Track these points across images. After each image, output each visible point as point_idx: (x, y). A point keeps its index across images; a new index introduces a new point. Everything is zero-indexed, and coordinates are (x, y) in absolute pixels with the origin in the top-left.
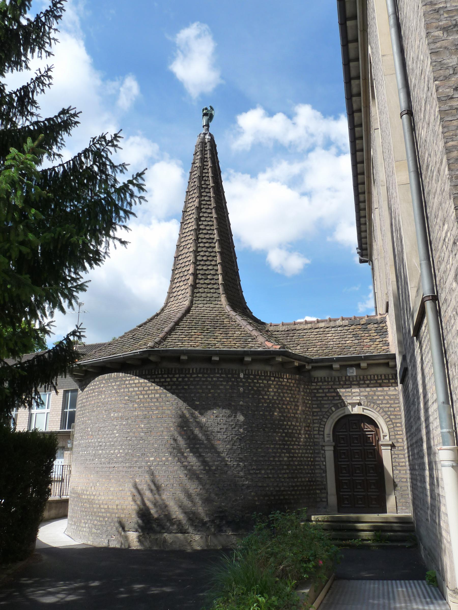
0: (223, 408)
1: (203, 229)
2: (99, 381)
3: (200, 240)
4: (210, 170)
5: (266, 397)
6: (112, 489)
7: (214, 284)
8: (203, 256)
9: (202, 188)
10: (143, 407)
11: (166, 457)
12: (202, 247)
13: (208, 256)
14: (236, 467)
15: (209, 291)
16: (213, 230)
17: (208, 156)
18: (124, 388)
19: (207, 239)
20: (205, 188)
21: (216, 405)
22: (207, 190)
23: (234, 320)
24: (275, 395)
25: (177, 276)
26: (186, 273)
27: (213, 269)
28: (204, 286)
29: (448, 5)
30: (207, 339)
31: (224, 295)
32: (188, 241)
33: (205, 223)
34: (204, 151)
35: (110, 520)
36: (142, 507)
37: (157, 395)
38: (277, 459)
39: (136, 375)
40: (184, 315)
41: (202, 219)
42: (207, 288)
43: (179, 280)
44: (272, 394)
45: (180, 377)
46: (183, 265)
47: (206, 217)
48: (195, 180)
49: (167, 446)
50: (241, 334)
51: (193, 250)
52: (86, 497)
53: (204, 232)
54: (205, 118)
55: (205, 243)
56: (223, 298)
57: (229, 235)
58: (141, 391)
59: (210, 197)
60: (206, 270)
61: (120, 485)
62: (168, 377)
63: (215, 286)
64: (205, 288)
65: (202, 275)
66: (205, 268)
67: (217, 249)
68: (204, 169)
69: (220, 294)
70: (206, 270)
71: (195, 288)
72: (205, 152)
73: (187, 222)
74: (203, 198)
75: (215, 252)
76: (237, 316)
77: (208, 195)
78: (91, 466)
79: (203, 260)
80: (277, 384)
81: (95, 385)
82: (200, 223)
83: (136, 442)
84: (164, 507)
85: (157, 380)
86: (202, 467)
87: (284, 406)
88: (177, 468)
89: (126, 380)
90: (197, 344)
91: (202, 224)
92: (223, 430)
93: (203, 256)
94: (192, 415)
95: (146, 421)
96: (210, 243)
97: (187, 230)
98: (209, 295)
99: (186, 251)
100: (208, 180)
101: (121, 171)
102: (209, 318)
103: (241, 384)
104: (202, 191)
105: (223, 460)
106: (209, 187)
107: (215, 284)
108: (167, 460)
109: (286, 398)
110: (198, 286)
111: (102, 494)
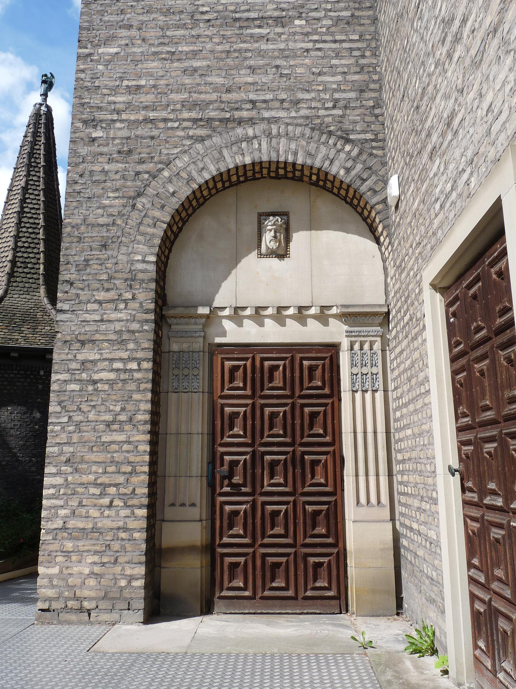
0: (19, 405)
3: (23, 225)
4: (42, 146)
7: (34, 274)
8: (24, 242)
9: (32, 166)
12: (25, 232)
13: (30, 243)
14: (29, 462)
15: (28, 280)
16: (39, 214)
17: (42, 130)
19: (32, 223)
20: (35, 167)
22: (36, 169)
23: (48, 314)
27: (35, 257)
28: (22, 275)
29: (92, 102)
30: (11, 334)
31: (44, 287)
32: (10, 224)
33: (30, 206)
34: (37, 124)
41: (28, 201)
42: (26, 277)
47: (33, 199)
48: (24, 156)
50: (51, 330)
51: (14, 235)
53: (29, 215)
54: (44, 86)
55: (28, 228)
57: (59, 221)
59: (39, 177)
60: (26, 258)
63: (35, 276)
64: (23, 278)
65: (22, 263)
66: (25, 255)
67: (41, 236)
68: (36, 145)
69: (39, 284)
70: (26, 258)
71: (12, 277)
72: (38, 125)
73: (12, 203)
74: (31, 178)
75: (39, 239)
77: (37, 174)
79: (23, 247)
82: (25, 205)
91: (27, 207)
93: (24, 242)
97: (10, 212)
98: (27, 285)
99: (6, 234)
100: (39, 158)
102: (22, 310)
103: (41, 381)
104: (31, 169)
105: (15, 455)
106: (39, 166)
110: (15, 274)
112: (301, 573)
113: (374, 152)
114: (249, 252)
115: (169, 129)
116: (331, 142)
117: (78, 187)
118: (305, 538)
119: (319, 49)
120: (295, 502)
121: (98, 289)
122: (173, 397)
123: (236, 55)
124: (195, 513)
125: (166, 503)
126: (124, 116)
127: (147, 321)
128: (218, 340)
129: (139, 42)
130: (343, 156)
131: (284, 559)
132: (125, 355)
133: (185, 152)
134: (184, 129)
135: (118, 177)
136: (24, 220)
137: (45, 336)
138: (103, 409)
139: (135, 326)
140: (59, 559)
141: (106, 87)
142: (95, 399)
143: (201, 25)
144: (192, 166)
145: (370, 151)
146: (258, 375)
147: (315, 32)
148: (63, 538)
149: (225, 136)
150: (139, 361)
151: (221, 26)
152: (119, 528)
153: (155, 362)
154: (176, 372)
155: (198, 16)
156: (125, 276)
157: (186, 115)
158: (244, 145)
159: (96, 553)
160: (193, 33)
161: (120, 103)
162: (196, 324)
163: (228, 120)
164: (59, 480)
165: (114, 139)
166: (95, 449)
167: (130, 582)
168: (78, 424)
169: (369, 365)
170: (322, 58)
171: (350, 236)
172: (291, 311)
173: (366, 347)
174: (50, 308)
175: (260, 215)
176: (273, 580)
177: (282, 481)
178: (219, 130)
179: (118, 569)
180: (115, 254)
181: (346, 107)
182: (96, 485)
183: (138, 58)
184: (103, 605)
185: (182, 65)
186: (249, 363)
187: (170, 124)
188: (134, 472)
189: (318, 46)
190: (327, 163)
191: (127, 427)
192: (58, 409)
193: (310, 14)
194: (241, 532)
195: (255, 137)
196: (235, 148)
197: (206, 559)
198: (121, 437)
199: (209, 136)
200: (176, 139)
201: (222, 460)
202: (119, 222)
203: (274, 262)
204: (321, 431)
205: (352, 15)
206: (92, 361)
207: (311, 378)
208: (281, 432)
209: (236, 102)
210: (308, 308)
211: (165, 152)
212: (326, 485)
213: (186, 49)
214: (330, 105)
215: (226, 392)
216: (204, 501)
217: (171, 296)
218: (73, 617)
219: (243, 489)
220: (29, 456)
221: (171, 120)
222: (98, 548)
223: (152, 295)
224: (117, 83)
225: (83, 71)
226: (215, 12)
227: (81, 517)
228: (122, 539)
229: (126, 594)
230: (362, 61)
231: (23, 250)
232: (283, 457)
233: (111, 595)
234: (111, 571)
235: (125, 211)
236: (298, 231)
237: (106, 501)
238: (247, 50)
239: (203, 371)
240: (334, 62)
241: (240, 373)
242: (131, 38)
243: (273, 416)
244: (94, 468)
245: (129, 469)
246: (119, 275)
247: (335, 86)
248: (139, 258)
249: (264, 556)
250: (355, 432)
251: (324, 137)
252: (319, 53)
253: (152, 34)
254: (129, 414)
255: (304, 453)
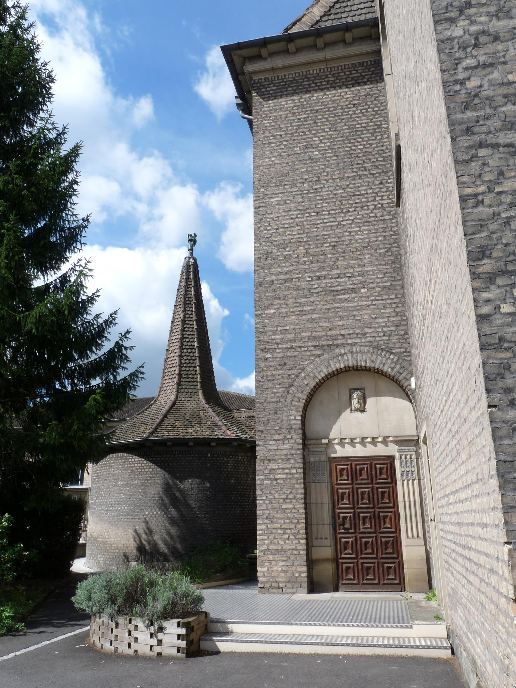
1: (187, 338)
2: (109, 458)
3: (184, 347)
5: (226, 470)
6: (120, 534)
7: (194, 382)
9: (187, 304)
10: (141, 477)
11: (157, 511)
12: (186, 352)
13: (190, 360)
17: (192, 276)
18: (128, 464)
19: (190, 346)
20: (189, 304)
21: (190, 476)
24: (232, 468)
25: (167, 374)
26: (173, 373)
28: (186, 383)
32: (175, 347)
33: (188, 333)
35: (118, 555)
36: (140, 545)
37: (151, 470)
38: (232, 512)
39: (136, 456)
40: (171, 408)
41: (186, 329)
43: (168, 377)
44: (230, 467)
45: (166, 457)
46: (171, 366)
47: (189, 328)
49: (158, 504)
52: (101, 540)
53: (187, 340)
55: (188, 349)
56: (200, 393)
58: (139, 467)
59: (192, 311)
60: (188, 371)
61: (125, 531)
62: (158, 457)
63: (195, 384)
65: (185, 375)
66: (187, 369)
67: (197, 354)
68: (188, 288)
70: (188, 371)
73: (175, 331)
74: (187, 313)
76: (209, 409)
77: (191, 309)
78: (105, 518)
79: (186, 363)
80: (234, 460)
81: (106, 461)
82: (184, 333)
83: (136, 502)
84: (154, 545)
85: (151, 459)
86: (180, 518)
87: (239, 476)
88: (163, 519)
89: (129, 459)
90: (179, 433)
92: (195, 493)
94: (175, 483)
95: (143, 487)
96: (192, 349)
97: (174, 338)
98: (190, 390)
99: (173, 354)
101: (130, 349)
104: (187, 306)
106: (192, 303)
107: (195, 381)
108: (157, 514)
109: (240, 470)
110: (181, 383)
111: (112, 537)
112: (381, 572)
113: (406, 358)
114: (346, 409)
115: (302, 351)
116: (383, 354)
117: (261, 384)
118: (382, 554)
119: (375, 305)
120: (376, 537)
121: (274, 434)
122: (313, 485)
123: (333, 310)
124: (328, 542)
125: (314, 538)
126: (280, 346)
127: (299, 449)
128: (333, 455)
129: (285, 306)
130: (389, 361)
131: (372, 565)
132: (290, 466)
133: (311, 363)
134: (310, 351)
135: (280, 377)
136: (185, 343)
137: (208, 429)
138: (281, 492)
139: (293, 452)
140: (267, 564)
141: (270, 331)
142: (277, 487)
143: (314, 295)
144: (315, 370)
145: (403, 358)
146: (354, 473)
147: (372, 295)
148: (268, 554)
149: (330, 353)
150: (296, 469)
151: (324, 295)
152: (293, 549)
153: (304, 468)
154: (313, 472)
155: (312, 291)
156: (287, 427)
157: (310, 344)
158: (340, 358)
159: (283, 561)
160: (311, 300)
161: (278, 339)
162: (321, 447)
163: (331, 345)
164: (264, 527)
165: (276, 358)
166: (279, 512)
167: (300, 574)
168: (270, 500)
169: (410, 466)
170: (376, 309)
171: (397, 399)
172: (369, 440)
173: (408, 457)
174: (208, 407)
175: (350, 390)
176: (367, 575)
177: (369, 526)
178: (327, 350)
179: (294, 568)
180: (281, 416)
181: (390, 335)
182: (281, 529)
183: (285, 315)
184: (288, 585)
185: (306, 318)
186: (349, 467)
187: (303, 349)
188: (298, 523)
189: (374, 303)
190: (382, 365)
191: (293, 501)
192: (261, 493)
193: (369, 286)
194: (351, 552)
195: (345, 354)
196: (335, 360)
197: (334, 565)
198: (291, 506)
199: (323, 354)
200: (306, 357)
201: (339, 516)
202: (282, 400)
203: (359, 414)
204: (388, 501)
205: (391, 285)
206: (274, 469)
207: (381, 474)
208: (367, 502)
209: (335, 336)
210: (377, 438)
211: (302, 363)
212: (391, 528)
213: (308, 308)
214: (382, 334)
215: (339, 482)
216: (332, 537)
217: (309, 434)
218: (275, 591)
219: (350, 531)
220: (204, 514)
221: (303, 347)
222: (284, 559)
223: (300, 436)
224: (276, 329)
225: (258, 323)
226: (321, 288)
227: (275, 544)
228: (295, 554)
229: (299, 580)
230: (397, 310)
231: (185, 365)
232: (369, 514)
233: (292, 580)
234: (291, 569)
235: (284, 395)
236: (369, 397)
237: (286, 536)
238: (338, 308)
239: (327, 471)
240: (383, 311)
241: (345, 472)
242: (280, 304)
243: (363, 493)
244: (280, 521)
245: (296, 521)
246: (284, 427)
247: (383, 324)
248: (293, 418)
249: (363, 563)
250: (404, 501)
251: (380, 351)
252: (375, 307)
253: (291, 301)
254: (294, 495)
255: (379, 512)
